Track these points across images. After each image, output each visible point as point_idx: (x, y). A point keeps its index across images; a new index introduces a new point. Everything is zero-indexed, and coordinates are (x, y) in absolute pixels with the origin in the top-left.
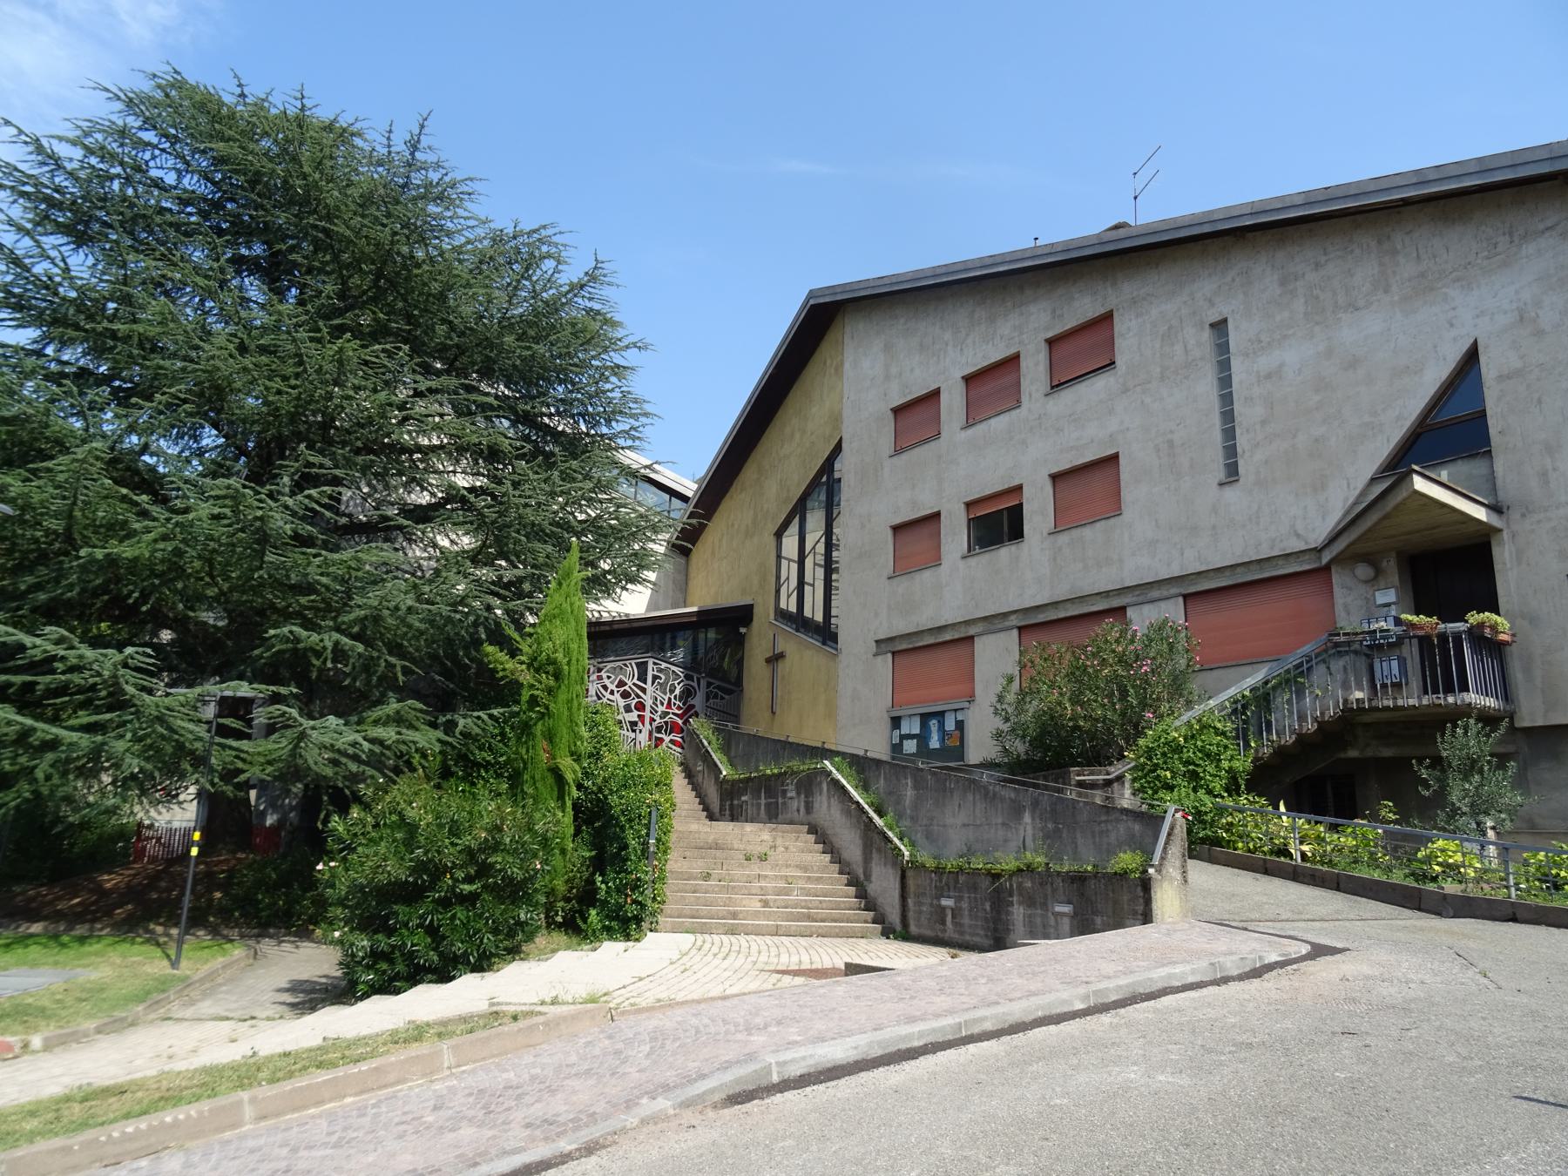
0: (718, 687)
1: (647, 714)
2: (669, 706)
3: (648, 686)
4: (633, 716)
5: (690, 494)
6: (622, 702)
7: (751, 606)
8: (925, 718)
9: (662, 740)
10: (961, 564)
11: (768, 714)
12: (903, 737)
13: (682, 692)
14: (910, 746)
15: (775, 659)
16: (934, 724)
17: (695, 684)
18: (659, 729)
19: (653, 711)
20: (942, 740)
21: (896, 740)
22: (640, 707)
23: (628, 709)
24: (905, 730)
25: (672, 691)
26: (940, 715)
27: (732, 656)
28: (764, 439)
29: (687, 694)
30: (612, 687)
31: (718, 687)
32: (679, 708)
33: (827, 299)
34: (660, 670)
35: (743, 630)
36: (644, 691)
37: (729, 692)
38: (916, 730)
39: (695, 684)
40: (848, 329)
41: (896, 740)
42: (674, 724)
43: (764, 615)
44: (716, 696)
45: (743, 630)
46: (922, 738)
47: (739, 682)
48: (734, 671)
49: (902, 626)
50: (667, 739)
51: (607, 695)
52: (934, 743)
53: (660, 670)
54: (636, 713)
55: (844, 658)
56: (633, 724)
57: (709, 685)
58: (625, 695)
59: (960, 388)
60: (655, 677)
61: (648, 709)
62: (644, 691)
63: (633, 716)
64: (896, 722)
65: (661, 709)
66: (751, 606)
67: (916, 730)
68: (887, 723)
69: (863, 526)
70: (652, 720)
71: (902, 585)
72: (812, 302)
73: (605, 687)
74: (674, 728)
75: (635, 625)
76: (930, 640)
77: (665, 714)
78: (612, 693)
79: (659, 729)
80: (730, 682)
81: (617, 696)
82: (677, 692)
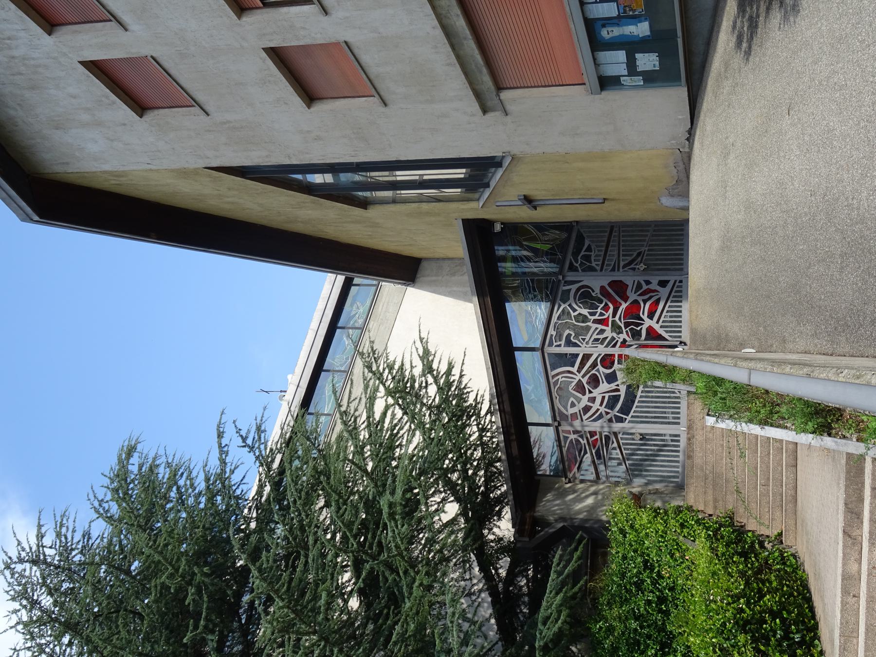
0: (576, 254)
2: (604, 322)
3: (581, 351)
5: (341, 279)
6: (604, 386)
8: (596, 44)
9: (650, 330)
10: (338, 14)
11: (607, 204)
12: (632, 69)
13: (586, 305)
14: (648, 61)
15: (528, 200)
16: (606, 34)
17: (574, 288)
18: (636, 335)
19: (613, 343)
20: (636, 19)
21: (639, 81)
22: (607, 361)
23: (611, 378)
24: (622, 70)
25: (585, 319)
26: (591, 26)
27: (534, 239)
29: (586, 297)
30: (585, 401)
31: (576, 254)
33: (23, 204)
34: (559, 336)
35: (498, 228)
36: (586, 357)
37: (580, 239)
39: (574, 288)
40: (46, 171)
42: (627, 313)
43: (475, 209)
44: (587, 258)
45: (498, 228)
46: (632, 47)
47: (566, 227)
48: (555, 234)
49: (455, 83)
50: (648, 323)
51: (596, 406)
52: (642, 29)
53: (559, 336)
54: (616, 366)
55: (516, 150)
57: (572, 268)
58: (595, 381)
59: (65, 34)
60: (569, 343)
61: (610, 351)
62: (586, 357)
64: (606, 83)
65: (609, 333)
68: (610, 95)
69: (318, 138)
70: (624, 344)
71: (390, 87)
72: (36, 218)
73: (587, 409)
74: (633, 313)
75: (503, 382)
76: (470, 46)
77: (616, 328)
78: (592, 400)
80: (568, 238)
81: (596, 393)
82: (585, 312)
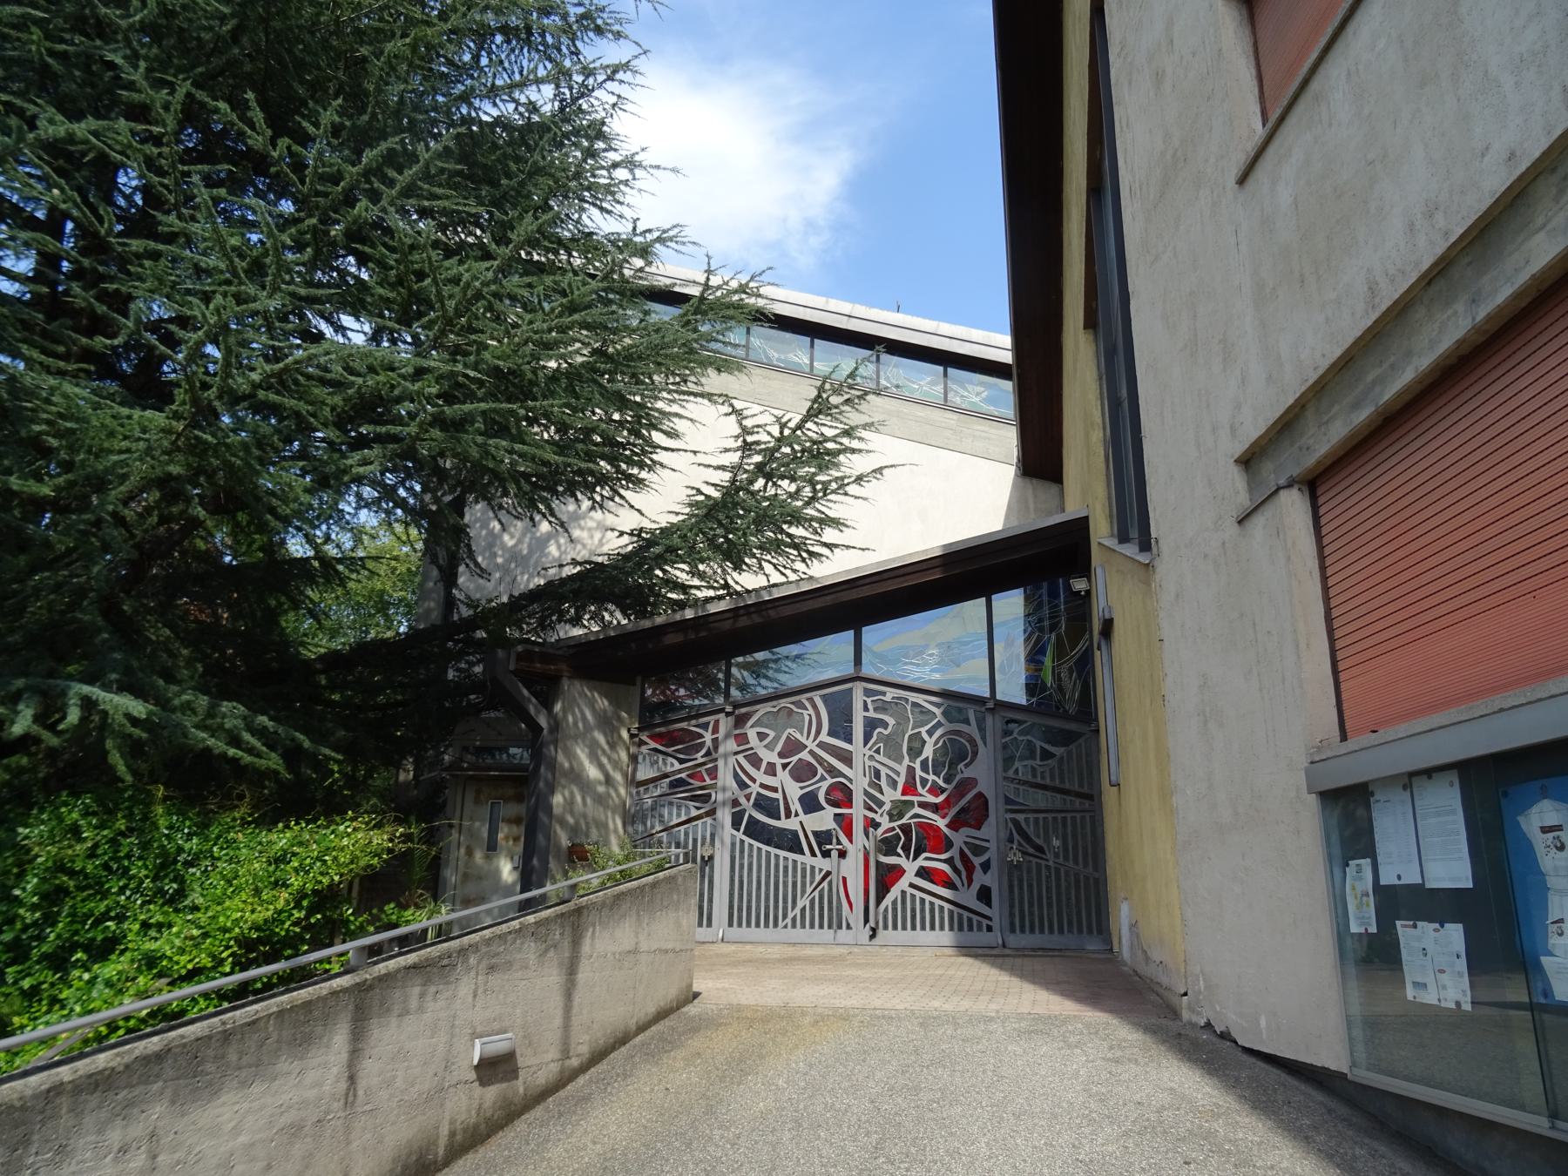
1: (858, 812)
2: (909, 789)
3: (857, 747)
4: (825, 819)
5: (1007, 357)
6: (794, 791)
7: (1087, 518)
9: (898, 872)
13: (941, 752)
17: (972, 730)
18: (888, 846)
19: (873, 803)
22: (841, 796)
23: (810, 803)
25: (915, 752)
28: (1066, 140)
30: (769, 756)
32: (936, 790)
34: (882, 707)
35: (1079, 585)
36: (847, 759)
37: (1067, 738)
38: (1452, 869)
39: (972, 730)
41: (1363, 919)
42: (928, 829)
45: (1079, 585)
50: (911, 867)
53: (882, 707)
54: (830, 811)
56: (823, 838)
58: (802, 773)
60: (871, 725)
61: (858, 799)
62: (847, 759)
63: (825, 819)
64: (1348, 811)
65: (890, 796)
66: (1087, 518)
67: (1452, 869)
68: (1304, 829)
73: (755, 761)
74: (929, 840)
75: (788, 611)
77: (898, 810)
78: (771, 770)
79: (888, 846)
80: (1066, 716)
81: (783, 777)
82: (928, 752)
